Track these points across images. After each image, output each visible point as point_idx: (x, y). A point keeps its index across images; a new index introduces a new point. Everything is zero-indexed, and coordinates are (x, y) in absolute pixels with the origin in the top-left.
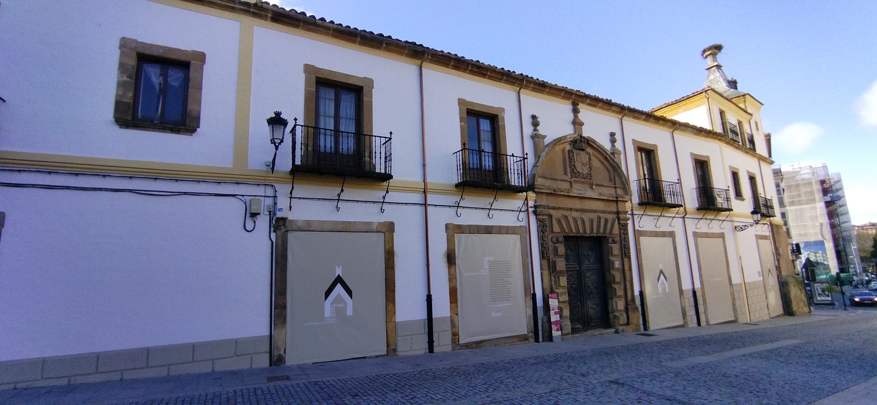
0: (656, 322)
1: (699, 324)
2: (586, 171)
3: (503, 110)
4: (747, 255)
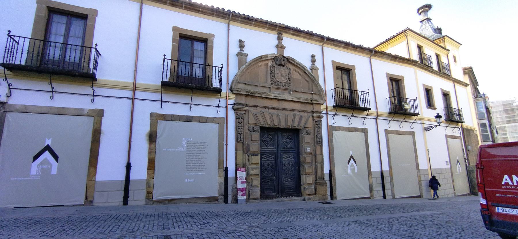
0: (341, 193)
1: (384, 197)
2: (284, 80)
3: (213, 35)
4: (437, 150)
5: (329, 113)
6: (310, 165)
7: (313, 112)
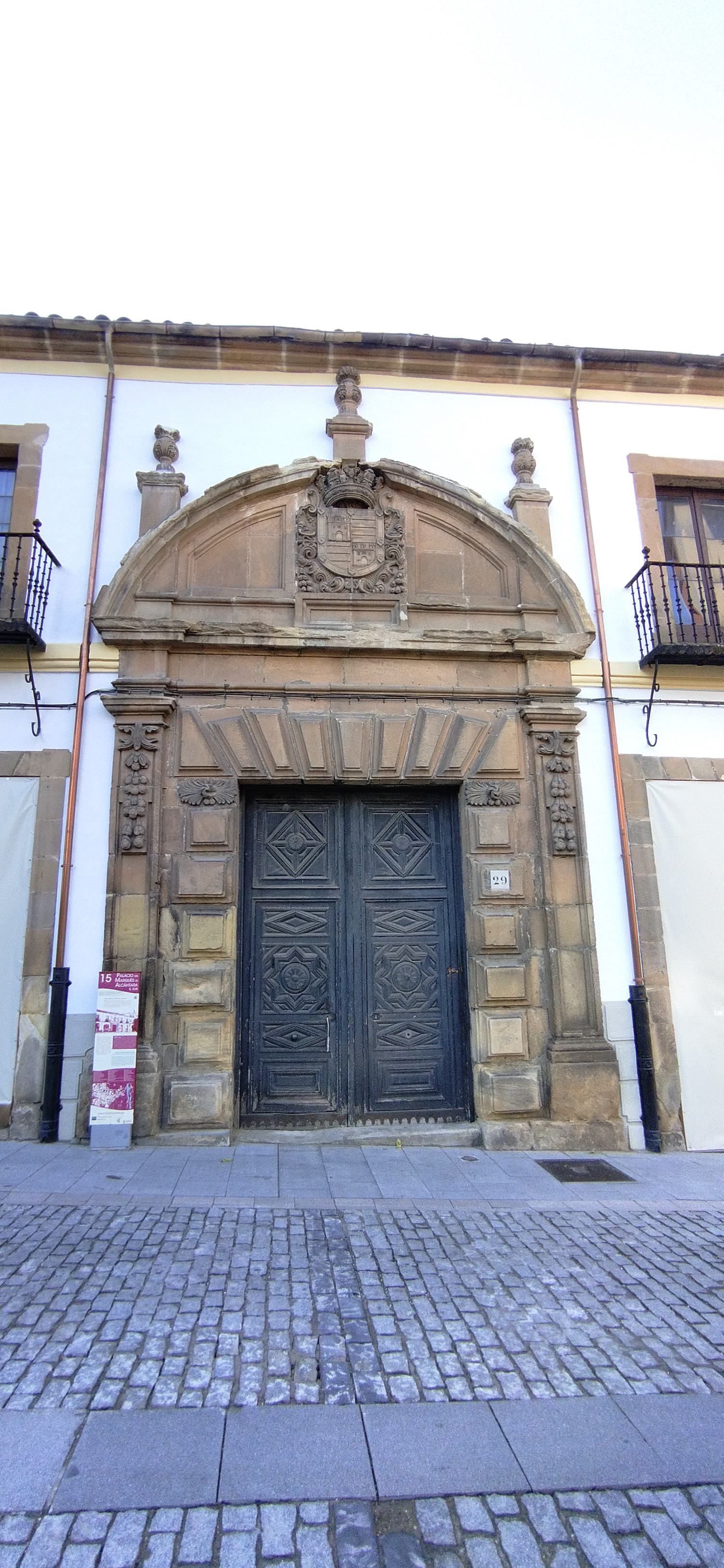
5: (616, 693)
6: (513, 961)
7: (526, 697)
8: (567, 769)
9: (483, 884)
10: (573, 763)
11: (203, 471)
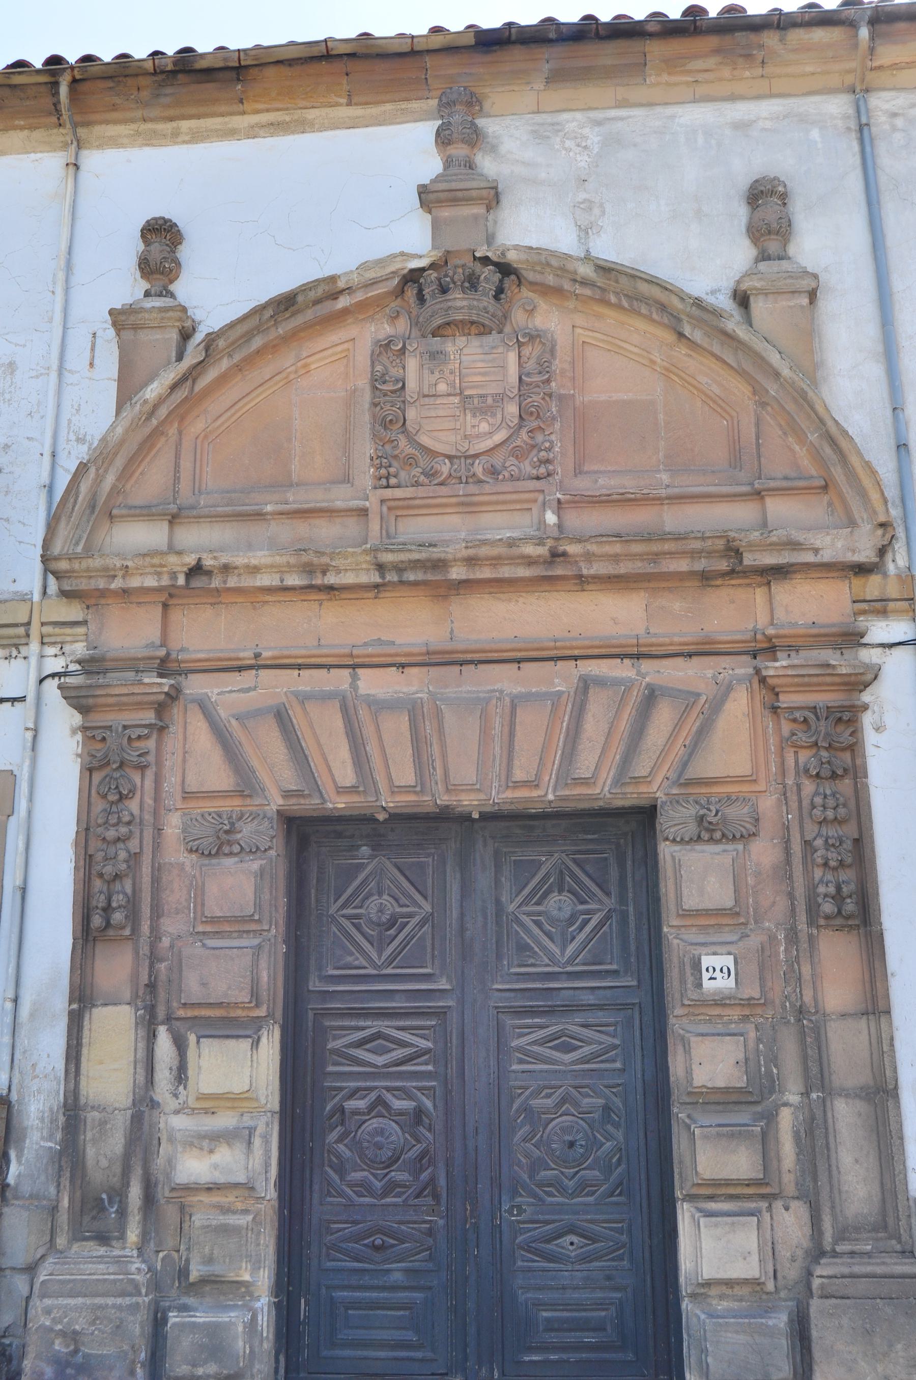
8: (840, 772)
9: (690, 979)
10: (853, 759)
11: (216, 293)
